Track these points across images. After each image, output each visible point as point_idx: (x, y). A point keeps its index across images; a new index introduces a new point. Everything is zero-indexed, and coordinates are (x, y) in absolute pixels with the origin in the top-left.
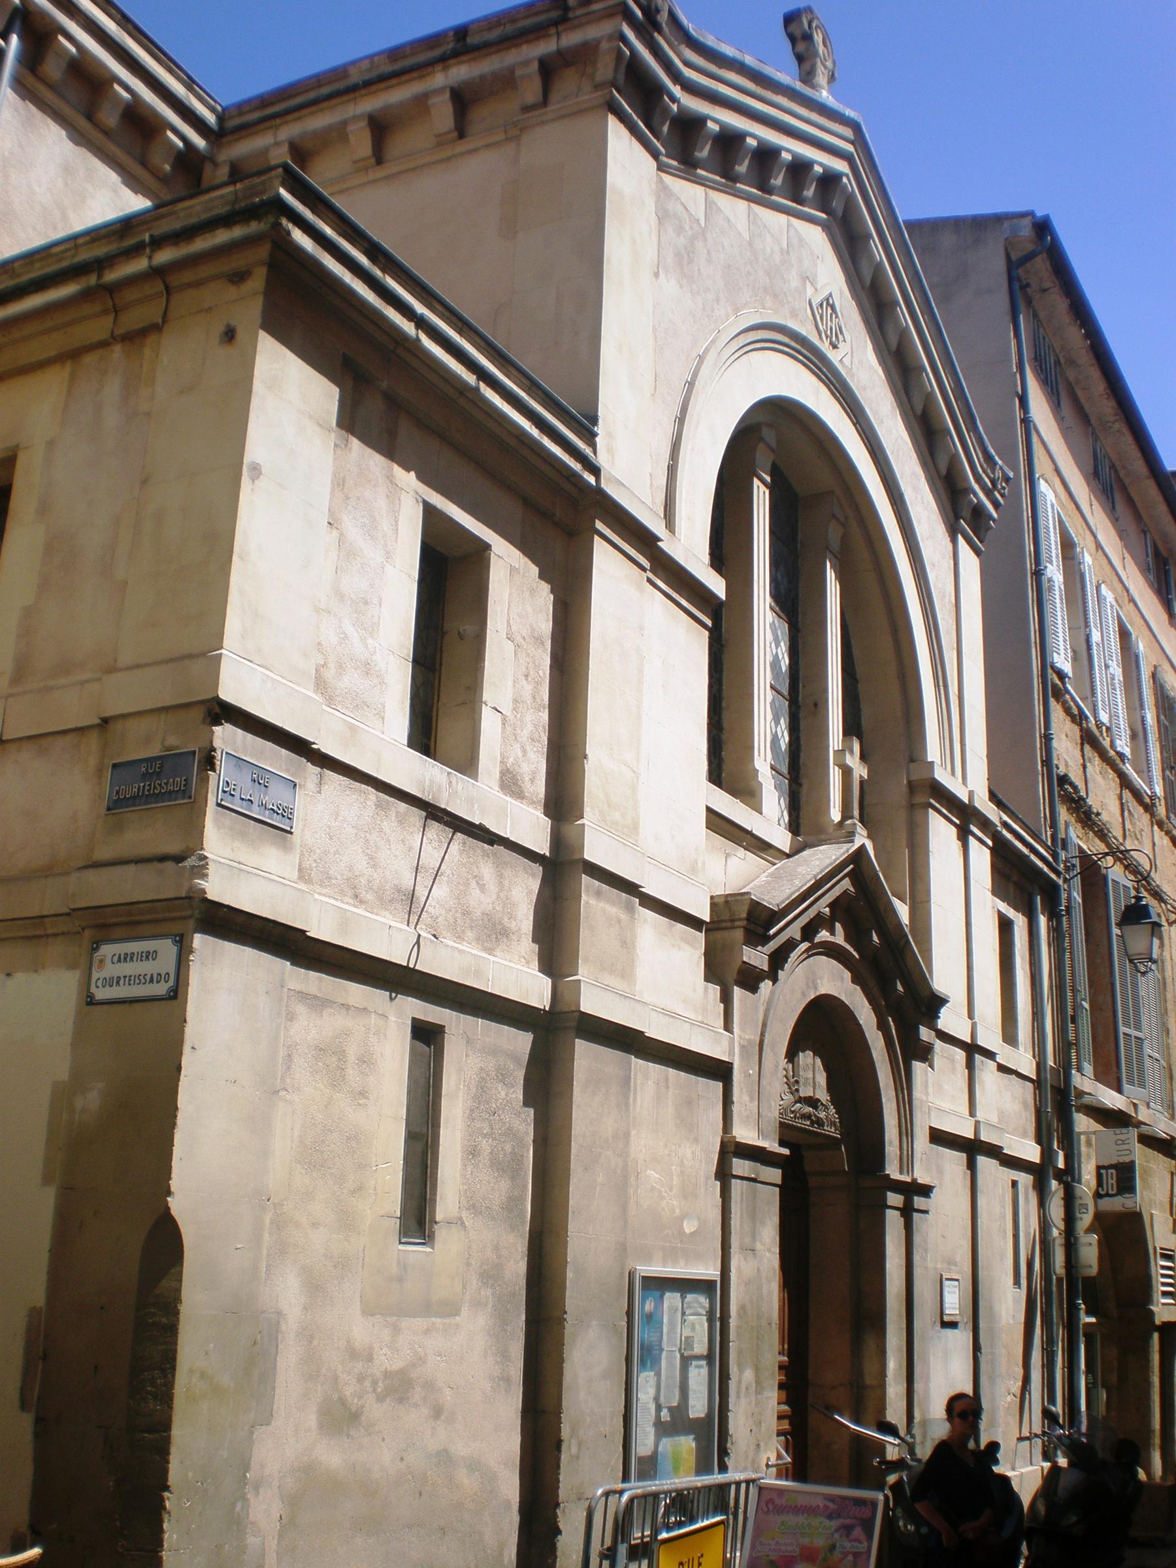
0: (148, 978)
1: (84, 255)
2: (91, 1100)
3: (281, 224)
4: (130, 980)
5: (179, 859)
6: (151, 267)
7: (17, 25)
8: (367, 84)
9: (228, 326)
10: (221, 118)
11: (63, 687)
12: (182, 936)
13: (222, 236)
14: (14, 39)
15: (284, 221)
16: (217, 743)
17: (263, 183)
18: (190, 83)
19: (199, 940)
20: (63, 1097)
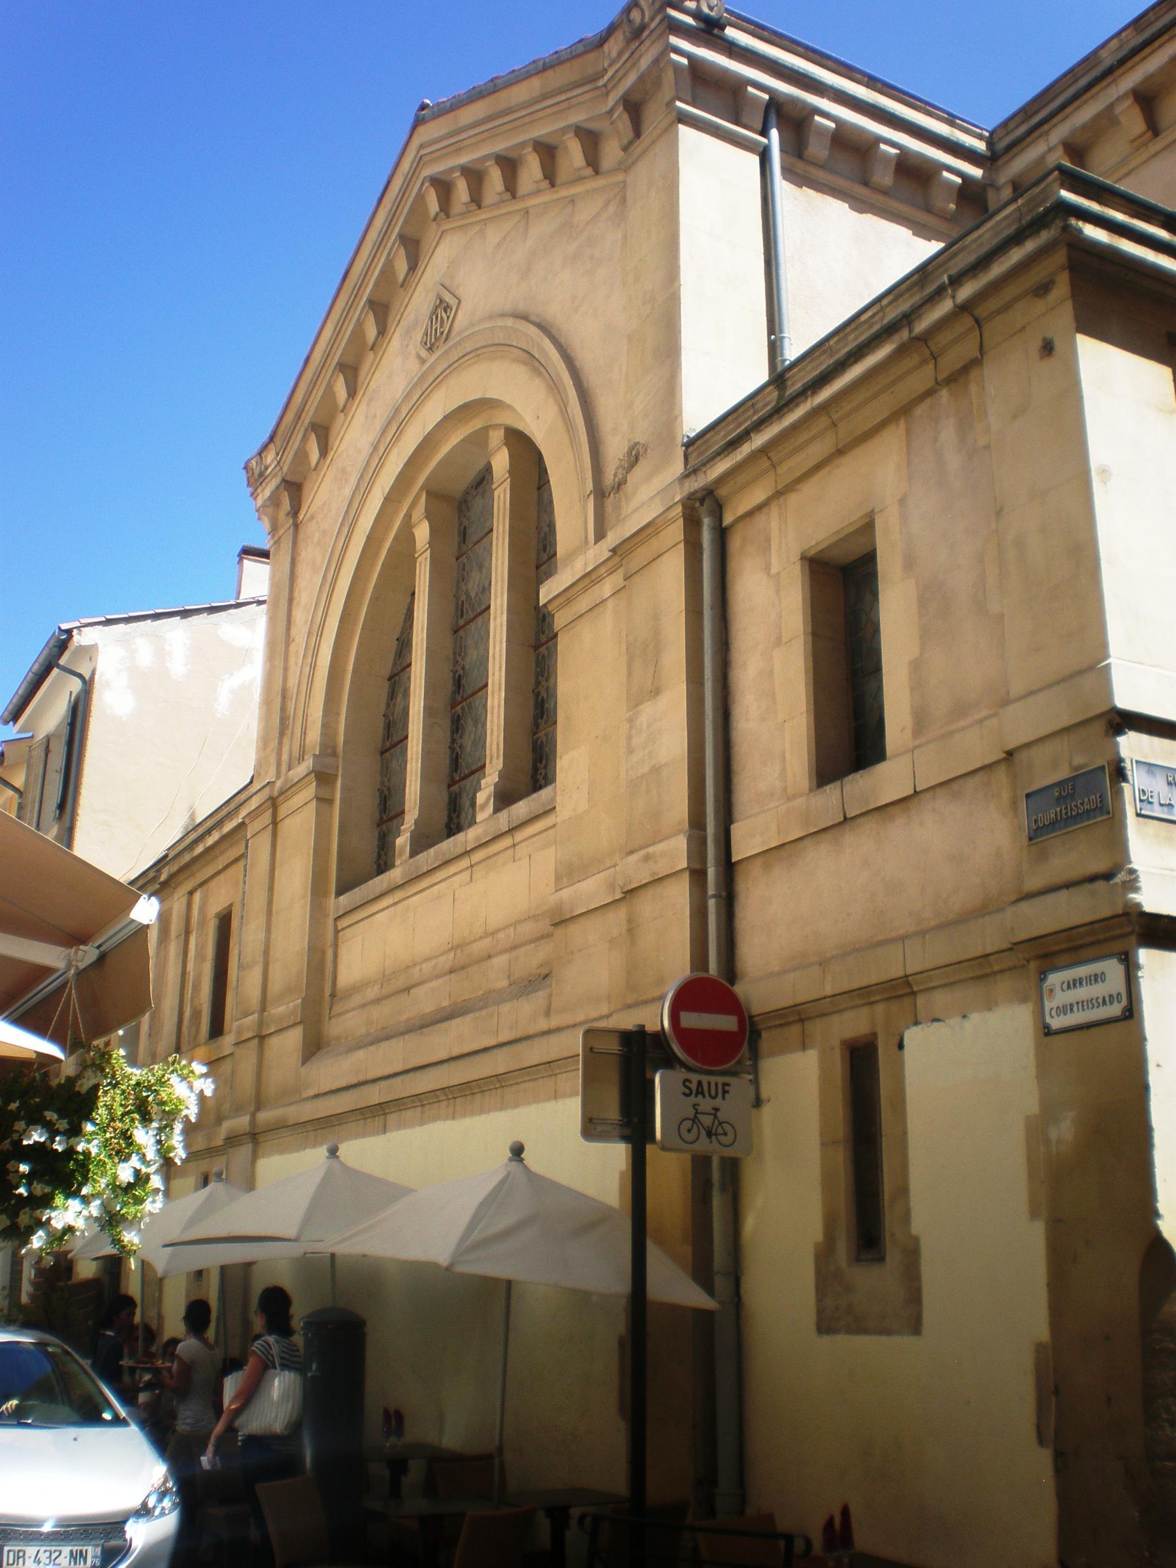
0: (1100, 1000)
1: (892, 315)
2: (1065, 1130)
3: (1070, 226)
4: (1083, 1005)
5: (1108, 876)
6: (956, 306)
7: (773, 119)
8: (1122, 62)
9: (1044, 339)
10: (990, 143)
11: (963, 729)
12: (1126, 954)
13: (1016, 255)
14: (774, 133)
15: (1073, 221)
16: (1124, 753)
17: (1043, 191)
18: (951, 120)
19: (1145, 955)
20: (1037, 1130)
